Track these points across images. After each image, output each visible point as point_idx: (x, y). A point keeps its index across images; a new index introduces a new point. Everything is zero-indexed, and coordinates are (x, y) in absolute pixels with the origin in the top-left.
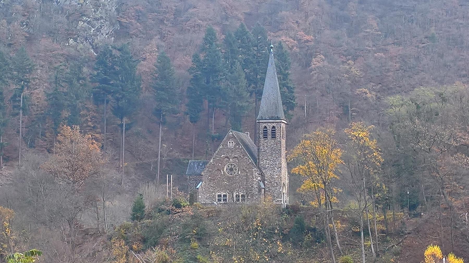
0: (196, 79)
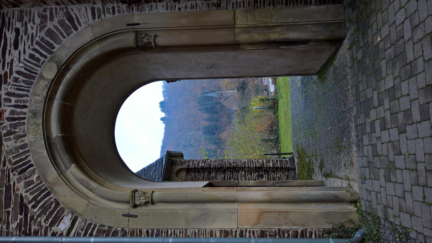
0: (209, 112)
